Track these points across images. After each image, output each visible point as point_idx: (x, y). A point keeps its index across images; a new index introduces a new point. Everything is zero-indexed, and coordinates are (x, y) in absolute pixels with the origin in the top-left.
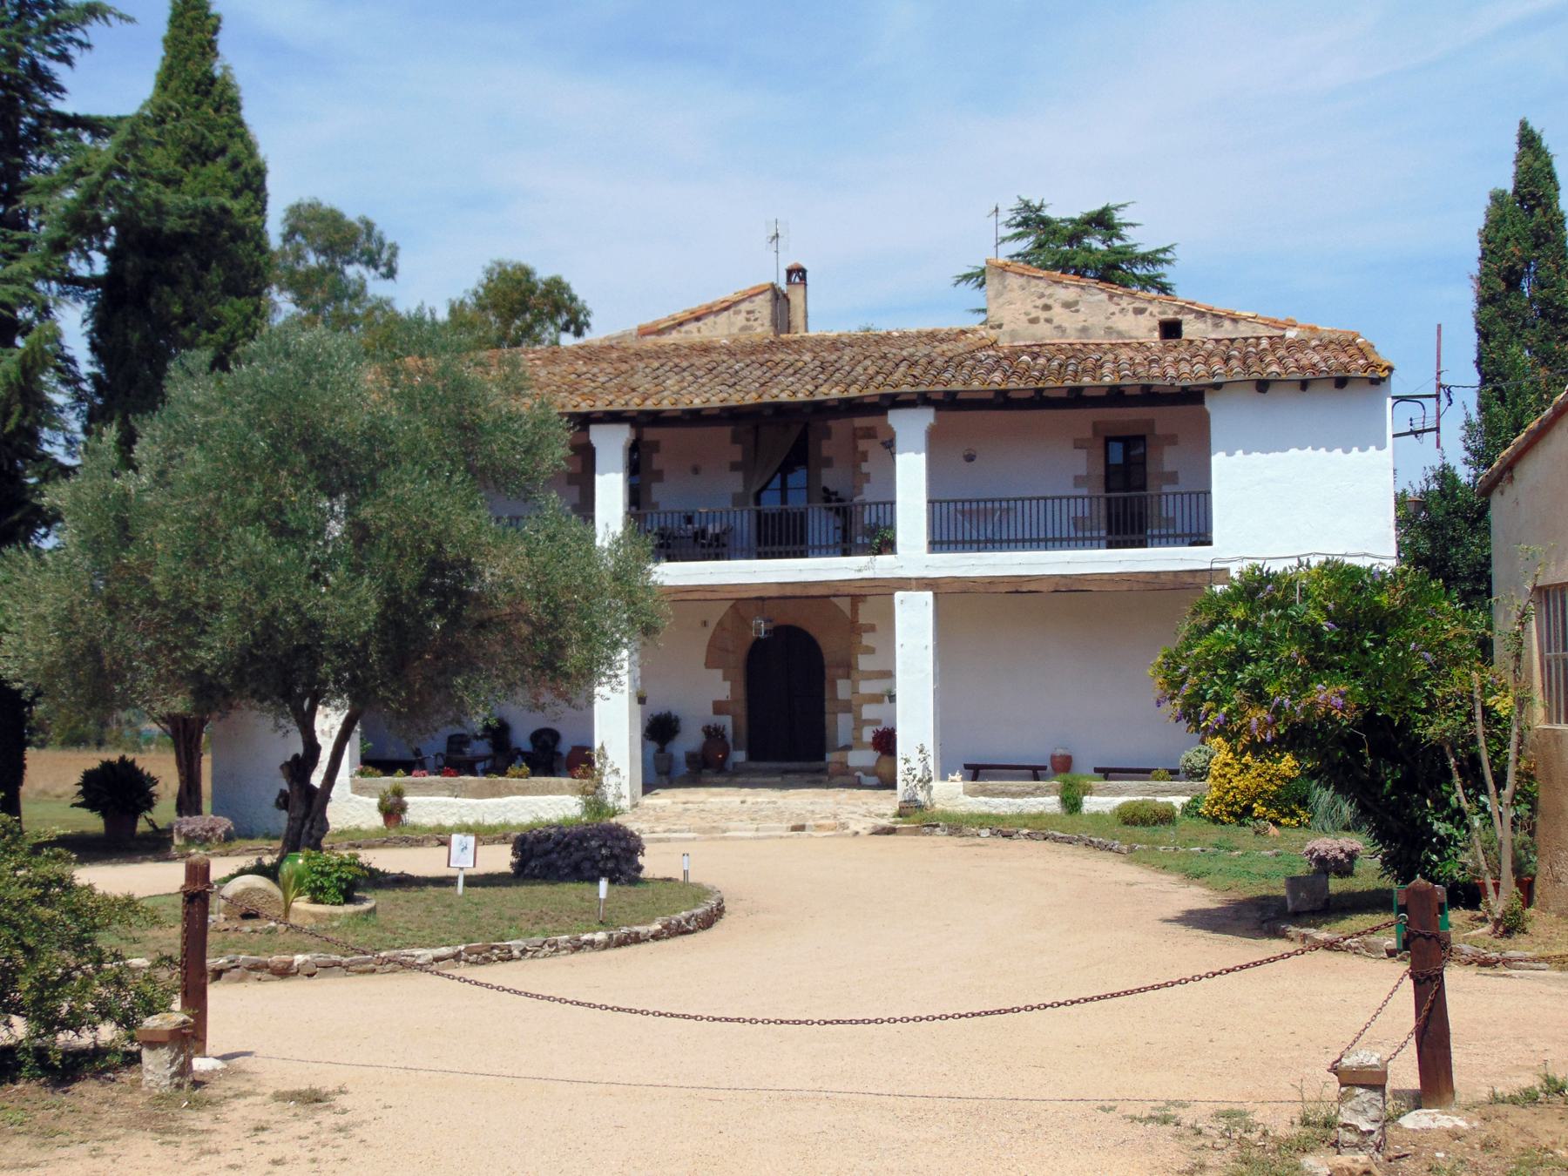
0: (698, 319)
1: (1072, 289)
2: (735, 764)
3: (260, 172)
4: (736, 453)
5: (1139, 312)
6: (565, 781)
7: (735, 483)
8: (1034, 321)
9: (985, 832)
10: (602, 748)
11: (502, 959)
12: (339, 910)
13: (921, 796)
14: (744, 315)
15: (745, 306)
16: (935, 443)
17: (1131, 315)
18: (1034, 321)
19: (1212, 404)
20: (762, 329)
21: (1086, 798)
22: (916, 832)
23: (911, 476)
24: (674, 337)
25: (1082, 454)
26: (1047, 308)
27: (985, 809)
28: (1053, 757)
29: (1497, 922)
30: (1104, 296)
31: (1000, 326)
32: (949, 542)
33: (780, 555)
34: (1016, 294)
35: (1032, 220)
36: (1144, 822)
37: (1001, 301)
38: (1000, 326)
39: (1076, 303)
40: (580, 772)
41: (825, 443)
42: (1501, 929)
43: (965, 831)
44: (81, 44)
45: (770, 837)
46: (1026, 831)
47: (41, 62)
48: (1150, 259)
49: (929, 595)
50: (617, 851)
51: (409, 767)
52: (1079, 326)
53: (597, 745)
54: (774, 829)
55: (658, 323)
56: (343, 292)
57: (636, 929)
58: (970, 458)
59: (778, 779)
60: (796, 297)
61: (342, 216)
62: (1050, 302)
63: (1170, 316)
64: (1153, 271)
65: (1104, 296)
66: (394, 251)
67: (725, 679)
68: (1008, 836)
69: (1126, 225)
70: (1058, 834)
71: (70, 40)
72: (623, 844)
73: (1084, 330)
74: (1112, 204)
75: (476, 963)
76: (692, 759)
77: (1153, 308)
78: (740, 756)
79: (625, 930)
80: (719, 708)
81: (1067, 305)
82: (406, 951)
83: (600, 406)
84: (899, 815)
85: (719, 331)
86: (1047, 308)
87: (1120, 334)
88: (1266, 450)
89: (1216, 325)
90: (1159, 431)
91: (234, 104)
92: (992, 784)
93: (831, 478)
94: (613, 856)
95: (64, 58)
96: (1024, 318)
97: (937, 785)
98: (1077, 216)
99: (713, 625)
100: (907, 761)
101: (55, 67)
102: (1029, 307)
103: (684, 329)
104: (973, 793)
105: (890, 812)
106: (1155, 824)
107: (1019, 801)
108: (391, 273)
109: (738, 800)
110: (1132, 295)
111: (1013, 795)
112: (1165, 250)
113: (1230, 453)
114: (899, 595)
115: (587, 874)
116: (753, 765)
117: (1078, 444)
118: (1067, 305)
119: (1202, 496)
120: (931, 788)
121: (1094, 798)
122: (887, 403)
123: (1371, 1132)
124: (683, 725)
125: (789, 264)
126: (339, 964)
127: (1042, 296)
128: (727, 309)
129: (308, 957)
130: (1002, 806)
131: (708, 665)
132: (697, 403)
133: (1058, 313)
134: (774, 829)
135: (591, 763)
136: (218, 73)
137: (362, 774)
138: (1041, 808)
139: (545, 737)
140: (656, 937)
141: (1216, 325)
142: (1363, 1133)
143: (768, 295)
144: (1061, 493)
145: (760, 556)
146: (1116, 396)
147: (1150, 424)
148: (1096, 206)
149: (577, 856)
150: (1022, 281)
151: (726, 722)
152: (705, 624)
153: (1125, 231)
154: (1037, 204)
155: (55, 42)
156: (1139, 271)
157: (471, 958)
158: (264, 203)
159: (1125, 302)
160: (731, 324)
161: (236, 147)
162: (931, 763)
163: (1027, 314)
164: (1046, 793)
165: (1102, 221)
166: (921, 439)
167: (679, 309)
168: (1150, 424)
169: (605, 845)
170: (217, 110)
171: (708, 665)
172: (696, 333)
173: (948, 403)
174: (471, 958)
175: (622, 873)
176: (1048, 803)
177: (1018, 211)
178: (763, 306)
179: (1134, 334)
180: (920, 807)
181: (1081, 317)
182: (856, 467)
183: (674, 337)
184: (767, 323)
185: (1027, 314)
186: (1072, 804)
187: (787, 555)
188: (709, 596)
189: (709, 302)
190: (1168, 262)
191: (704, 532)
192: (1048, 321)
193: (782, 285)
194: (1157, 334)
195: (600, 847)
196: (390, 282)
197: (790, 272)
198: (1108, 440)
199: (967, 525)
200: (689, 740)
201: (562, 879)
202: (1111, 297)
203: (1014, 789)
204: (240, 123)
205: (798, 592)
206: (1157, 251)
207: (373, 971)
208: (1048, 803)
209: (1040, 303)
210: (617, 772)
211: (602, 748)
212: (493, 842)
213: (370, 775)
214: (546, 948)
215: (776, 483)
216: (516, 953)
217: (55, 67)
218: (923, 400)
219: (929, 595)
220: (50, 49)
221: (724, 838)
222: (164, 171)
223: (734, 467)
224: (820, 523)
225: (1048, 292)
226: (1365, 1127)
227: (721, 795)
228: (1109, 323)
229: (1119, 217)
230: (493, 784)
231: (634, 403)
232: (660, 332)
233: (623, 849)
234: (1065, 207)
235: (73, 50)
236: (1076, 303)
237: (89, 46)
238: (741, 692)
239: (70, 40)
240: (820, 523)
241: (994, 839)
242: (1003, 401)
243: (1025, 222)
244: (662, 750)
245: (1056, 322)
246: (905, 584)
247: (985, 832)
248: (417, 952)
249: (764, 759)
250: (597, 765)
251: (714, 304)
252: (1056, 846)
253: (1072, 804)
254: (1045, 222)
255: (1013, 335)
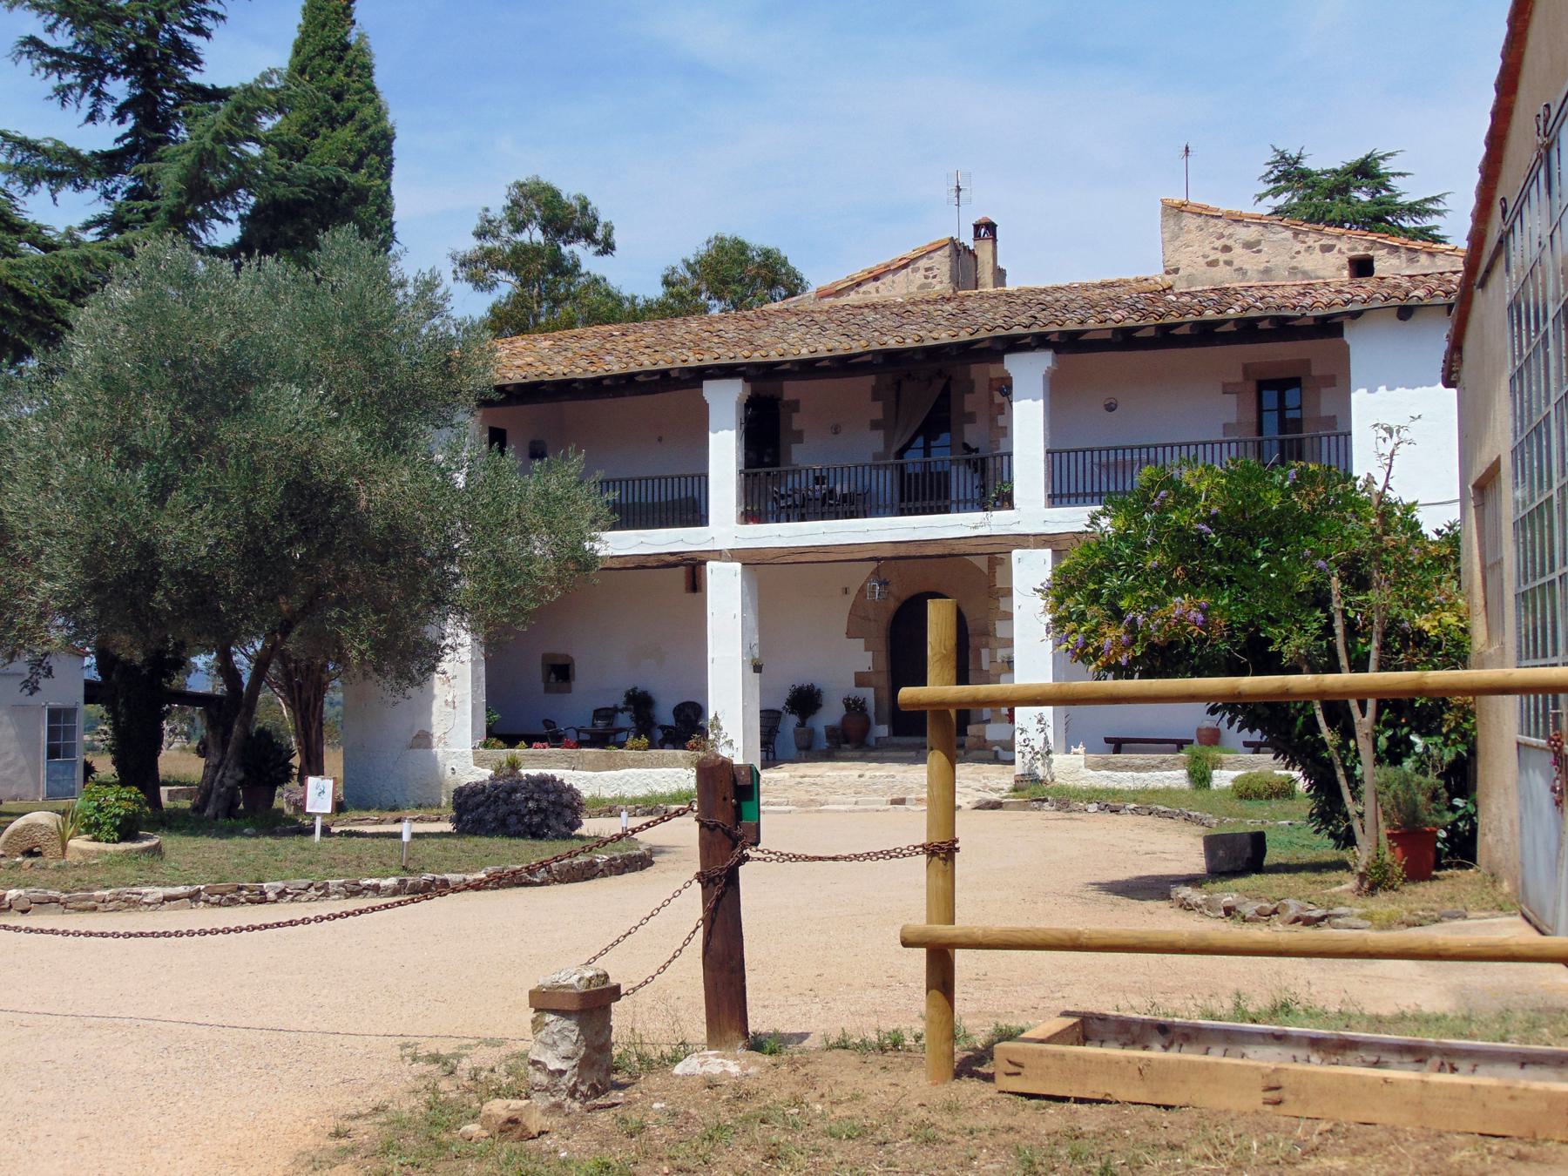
0: (876, 278)
1: (1253, 228)
2: (877, 739)
3: (387, 137)
4: (877, 410)
5: (1327, 249)
6: (680, 753)
7: (875, 442)
8: (1213, 264)
9: (1093, 807)
10: (716, 717)
11: (253, 902)
12: (111, 847)
13: (1041, 772)
14: (922, 272)
15: (923, 263)
16: (1057, 392)
17: (1317, 253)
18: (1213, 264)
19: (1352, 335)
20: (942, 285)
21: (1215, 772)
22: (1023, 806)
23: (1029, 426)
24: (853, 298)
25: (1232, 399)
26: (1227, 249)
27: (1139, 785)
28: (1199, 730)
29: (1362, 876)
30: (1289, 234)
31: (1176, 271)
32: (1077, 495)
33: (917, 513)
34: (1194, 236)
35: (1289, 173)
36: (1258, 796)
37: (1177, 243)
38: (1176, 271)
39: (1258, 242)
40: (692, 742)
41: (968, 397)
42: (1366, 885)
43: (1072, 806)
44: (215, 15)
45: (866, 810)
46: (1133, 806)
47: (181, 36)
48: (1415, 210)
49: (1047, 553)
50: (544, 804)
51: (530, 740)
52: (1261, 267)
53: (711, 716)
54: (874, 802)
55: (837, 283)
56: (563, 269)
57: (447, 876)
58: (1110, 408)
59: (913, 754)
60: (984, 251)
61: (556, 195)
62: (1230, 242)
63: (1361, 252)
64: (1428, 222)
65: (1289, 234)
66: (609, 229)
67: (867, 649)
68: (1115, 811)
69: (1393, 175)
70: (1162, 808)
71: (205, 12)
72: (552, 797)
73: (1267, 271)
74: (1380, 152)
75: (219, 904)
76: (832, 732)
77: (1343, 245)
78: (883, 730)
79: (428, 876)
80: (861, 680)
81: (1248, 245)
82: (135, 889)
83: (708, 360)
84: (1015, 790)
85: (896, 289)
86: (1227, 249)
87: (1305, 274)
88: (1411, 386)
89: (1411, 261)
90: (1316, 371)
91: (367, 69)
92: (1138, 759)
93: (972, 435)
94: (539, 810)
95: (199, 30)
96: (1202, 261)
97: (1058, 759)
98: (1338, 167)
99: (854, 592)
100: (1023, 731)
101: (195, 40)
102: (1207, 250)
103: (861, 289)
104: (1094, 767)
105: (1006, 787)
106: (1269, 797)
107: (1143, 775)
108: (607, 247)
109: (856, 773)
110: (1319, 231)
111: (1138, 769)
112: (1434, 199)
113: (1372, 390)
114: (1016, 553)
115: (512, 829)
116: (896, 740)
117: (1227, 389)
118: (1248, 245)
119: (1342, 438)
120: (1051, 761)
121: (1225, 772)
122: (999, 347)
123: (562, 1072)
124: (825, 697)
125: (976, 219)
126: (57, 901)
127: (1221, 236)
128: (905, 266)
129: (22, 892)
130: (1125, 780)
131: (849, 635)
132: (805, 353)
133: (1239, 255)
134: (874, 802)
135: (703, 732)
136: (352, 38)
137: (486, 746)
138: (1167, 783)
139: (689, 711)
140: (478, 886)
141: (1411, 261)
142: (552, 1073)
143: (946, 251)
144: (1213, 439)
145: (902, 513)
146: (1248, 330)
147: (1307, 363)
148: (1356, 155)
149: (503, 809)
150: (1200, 221)
151: (868, 694)
152: (846, 591)
153: (1394, 182)
154: (1294, 155)
155: (190, 15)
156: (1407, 223)
157: (212, 899)
158: (390, 167)
159: (1311, 239)
160: (909, 282)
161: (367, 111)
162: (1050, 732)
163: (1204, 256)
164: (1172, 767)
165: (1365, 170)
166: (1039, 384)
167: (857, 270)
168: (1307, 363)
169: (532, 798)
170: (348, 75)
171: (849, 635)
172: (872, 293)
173: (1069, 344)
174: (212, 899)
175: (549, 828)
176: (1175, 777)
177: (1275, 164)
178: (941, 263)
179: (1321, 274)
180: (1037, 781)
181: (1263, 257)
182: (993, 420)
183: (853, 298)
184: (946, 279)
185: (1204, 256)
186: (1200, 779)
187: (931, 512)
188: (822, 557)
189: (887, 260)
190: (1438, 213)
191: (831, 492)
192: (1228, 263)
193: (968, 239)
194: (1346, 273)
195: (527, 799)
196: (607, 258)
197: (977, 227)
198: (1262, 386)
199: (1104, 478)
200: (831, 714)
201: (490, 833)
202: (1296, 235)
203: (1138, 762)
204: (372, 89)
205: (913, 552)
206: (1426, 200)
207: (95, 909)
208: (1175, 777)
209: (1219, 244)
210: (730, 743)
211: (716, 717)
212: (599, 815)
213: (493, 747)
214: (312, 891)
215: (920, 441)
216: (271, 895)
217: (195, 40)
218: (1040, 342)
219: (1047, 553)
220: (186, 22)
221: (819, 811)
222: (286, 138)
223: (875, 425)
224: (961, 481)
225: (1226, 233)
226: (554, 1065)
227: (843, 769)
228: (1294, 263)
229: (1384, 167)
230: (609, 757)
231: (742, 355)
232: (838, 293)
233: (553, 803)
234: (1324, 159)
235: (208, 23)
236: (1258, 242)
237: (223, 18)
238: (883, 664)
239: (205, 12)
240: (961, 481)
241: (1100, 815)
242: (1125, 339)
243: (1285, 175)
244: (802, 724)
245: (1237, 264)
246: (1023, 541)
247: (1093, 807)
248: (145, 890)
249: (910, 734)
250: (711, 737)
251: (893, 262)
252: (1161, 822)
253: (1200, 779)
254: (1305, 175)
255: (1190, 279)
